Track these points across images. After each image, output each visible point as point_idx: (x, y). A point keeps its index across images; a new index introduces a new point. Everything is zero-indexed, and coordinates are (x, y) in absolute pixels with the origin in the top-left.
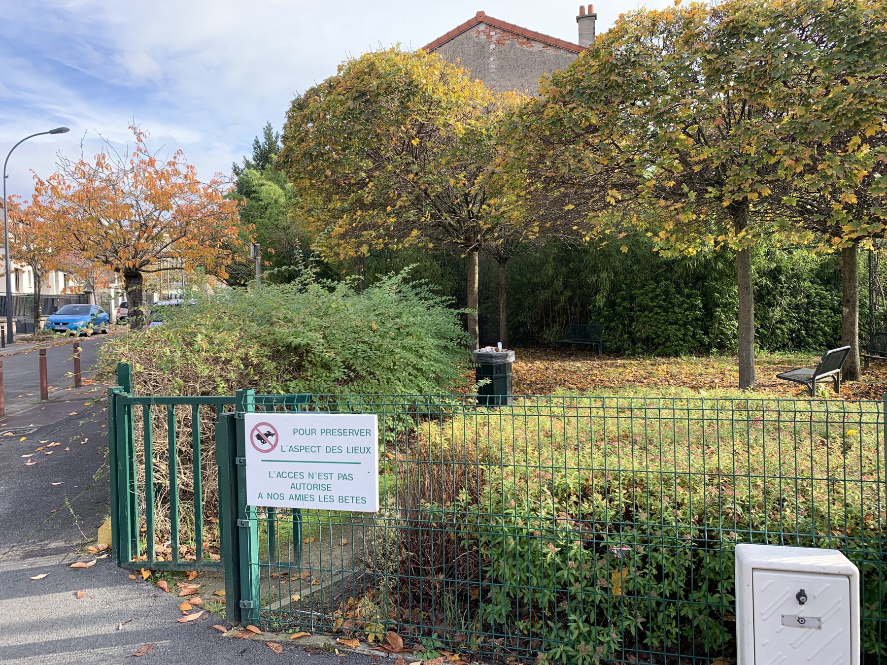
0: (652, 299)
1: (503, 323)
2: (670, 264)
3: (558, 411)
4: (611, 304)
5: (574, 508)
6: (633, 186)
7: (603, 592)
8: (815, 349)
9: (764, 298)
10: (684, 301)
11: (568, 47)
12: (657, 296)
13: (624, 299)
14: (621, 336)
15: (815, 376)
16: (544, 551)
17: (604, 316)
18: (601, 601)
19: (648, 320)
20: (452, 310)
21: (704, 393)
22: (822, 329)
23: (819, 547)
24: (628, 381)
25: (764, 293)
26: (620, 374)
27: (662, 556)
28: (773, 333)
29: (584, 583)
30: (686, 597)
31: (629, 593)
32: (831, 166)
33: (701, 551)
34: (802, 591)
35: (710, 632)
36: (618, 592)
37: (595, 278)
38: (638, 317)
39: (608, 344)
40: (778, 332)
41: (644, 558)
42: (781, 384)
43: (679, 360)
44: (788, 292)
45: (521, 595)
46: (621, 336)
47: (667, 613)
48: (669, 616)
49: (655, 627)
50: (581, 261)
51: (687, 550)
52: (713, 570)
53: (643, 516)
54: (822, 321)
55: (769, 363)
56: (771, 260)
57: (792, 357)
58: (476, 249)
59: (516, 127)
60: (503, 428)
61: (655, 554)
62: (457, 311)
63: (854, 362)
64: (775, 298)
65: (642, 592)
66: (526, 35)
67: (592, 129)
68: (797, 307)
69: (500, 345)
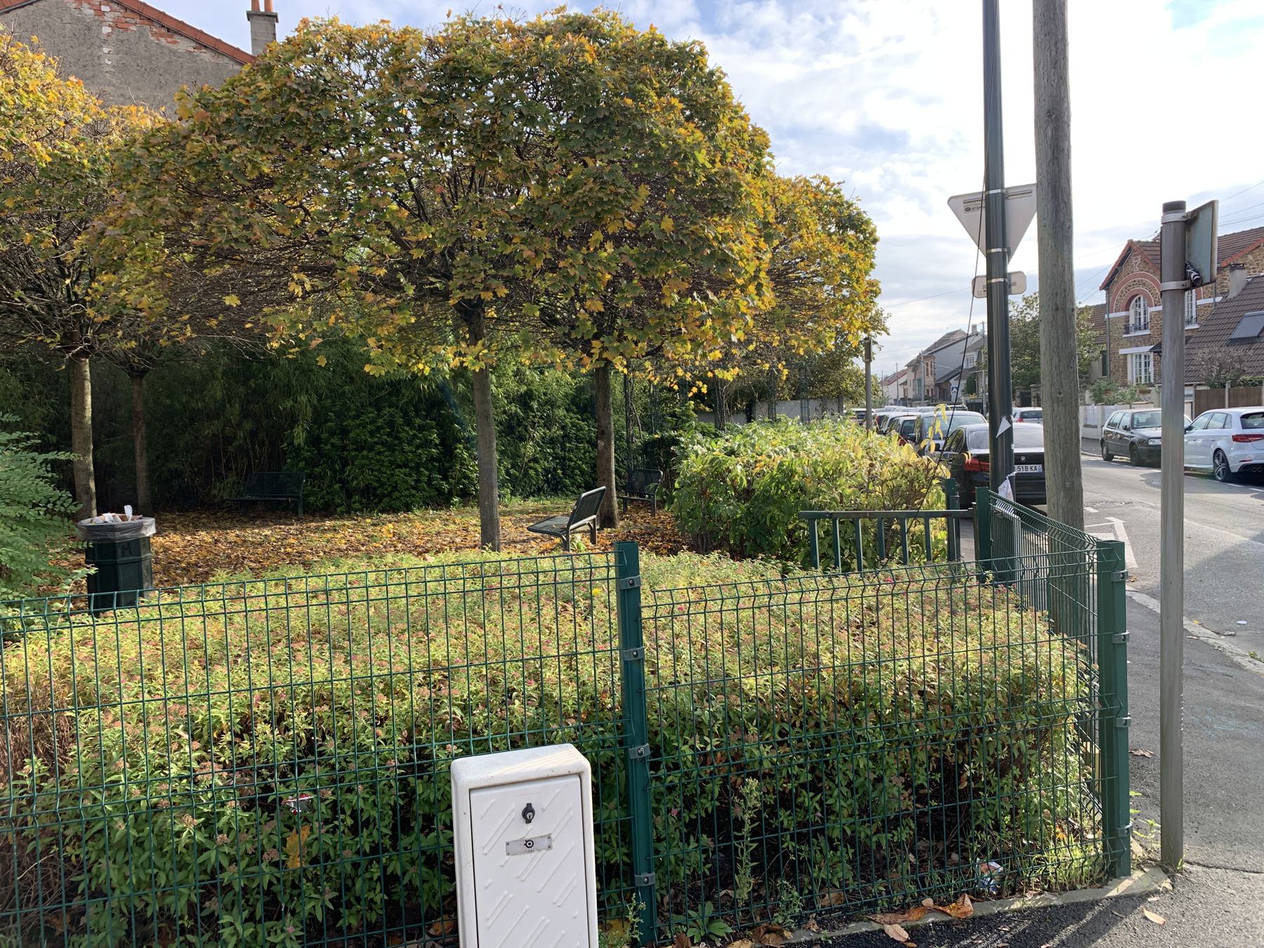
0: (372, 434)
1: (142, 475)
2: (395, 386)
3: (215, 606)
4: (314, 441)
5: (228, 753)
6: (330, 270)
7: (274, 869)
8: (573, 492)
9: (513, 430)
10: (415, 435)
11: (235, 55)
12: (379, 428)
13: (332, 434)
14: (330, 486)
15: (569, 525)
16: (176, 828)
17: (305, 459)
18: (270, 884)
19: (367, 462)
20: (35, 454)
21: (431, 559)
22: (579, 467)
23: (552, 743)
24: (339, 550)
25: (514, 423)
26: (328, 541)
27: (359, 798)
28: (526, 474)
29: (243, 864)
30: (394, 847)
31: (314, 861)
32: (573, 264)
33: (411, 779)
34: (529, 805)
35: (426, 886)
36: (295, 864)
37: (289, 403)
38: (355, 458)
39: (312, 499)
40: (532, 472)
41: (334, 806)
42: (534, 539)
43: (411, 516)
44: (542, 422)
45: (140, 906)
46: (330, 486)
47: (368, 875)
48: (371, 879)
49: (352, 900)
50: (267, 376)
51: (392, 782)
52: (427, 801)
53: (330, 746)
54: (579, 458)
55: (521, 512)
56: (521, 382)
57: (548, 503)
58: (84, 353)
59: (139, 165)
60: (121, 642)
61: (349, 796)
62: (43, 456)
63: (611, 506)
64: (526, 430)
65: (332, 854)
66: (166, 23)
67: (265, 182)
68: (552, 442)
69: (128, 509)
